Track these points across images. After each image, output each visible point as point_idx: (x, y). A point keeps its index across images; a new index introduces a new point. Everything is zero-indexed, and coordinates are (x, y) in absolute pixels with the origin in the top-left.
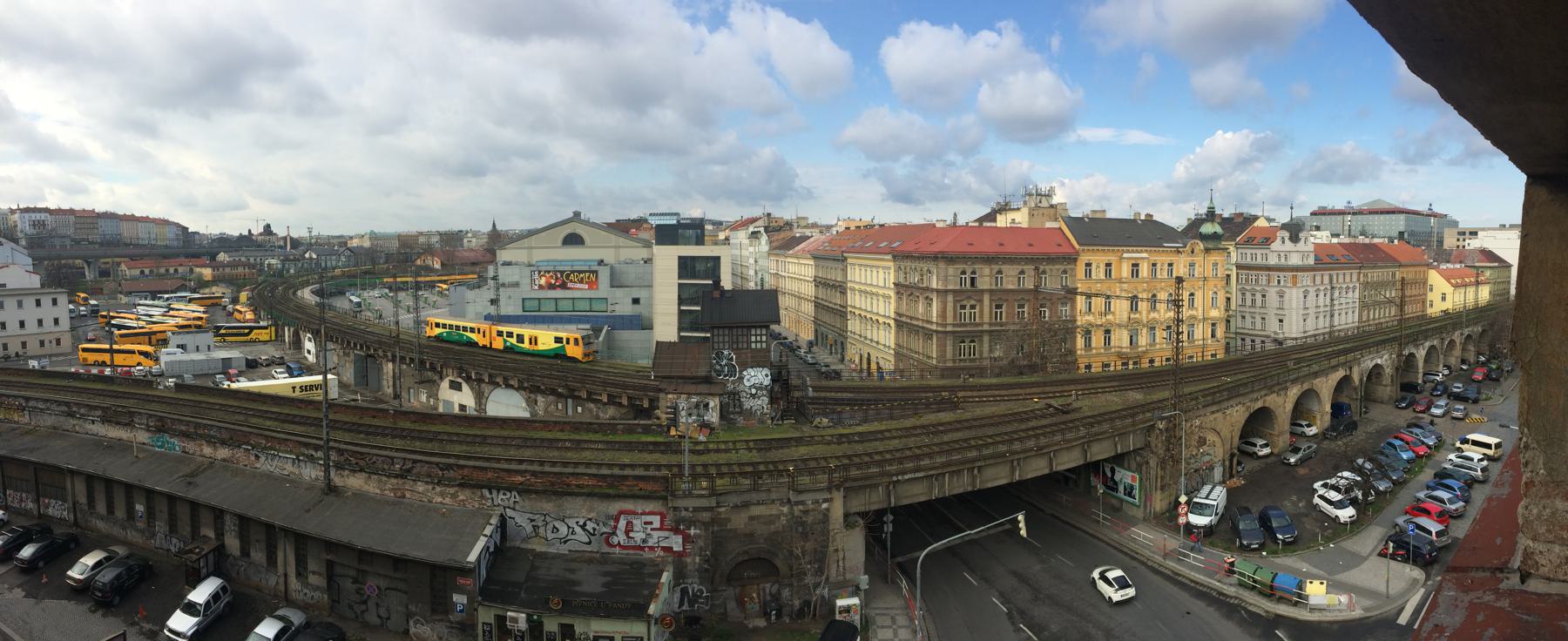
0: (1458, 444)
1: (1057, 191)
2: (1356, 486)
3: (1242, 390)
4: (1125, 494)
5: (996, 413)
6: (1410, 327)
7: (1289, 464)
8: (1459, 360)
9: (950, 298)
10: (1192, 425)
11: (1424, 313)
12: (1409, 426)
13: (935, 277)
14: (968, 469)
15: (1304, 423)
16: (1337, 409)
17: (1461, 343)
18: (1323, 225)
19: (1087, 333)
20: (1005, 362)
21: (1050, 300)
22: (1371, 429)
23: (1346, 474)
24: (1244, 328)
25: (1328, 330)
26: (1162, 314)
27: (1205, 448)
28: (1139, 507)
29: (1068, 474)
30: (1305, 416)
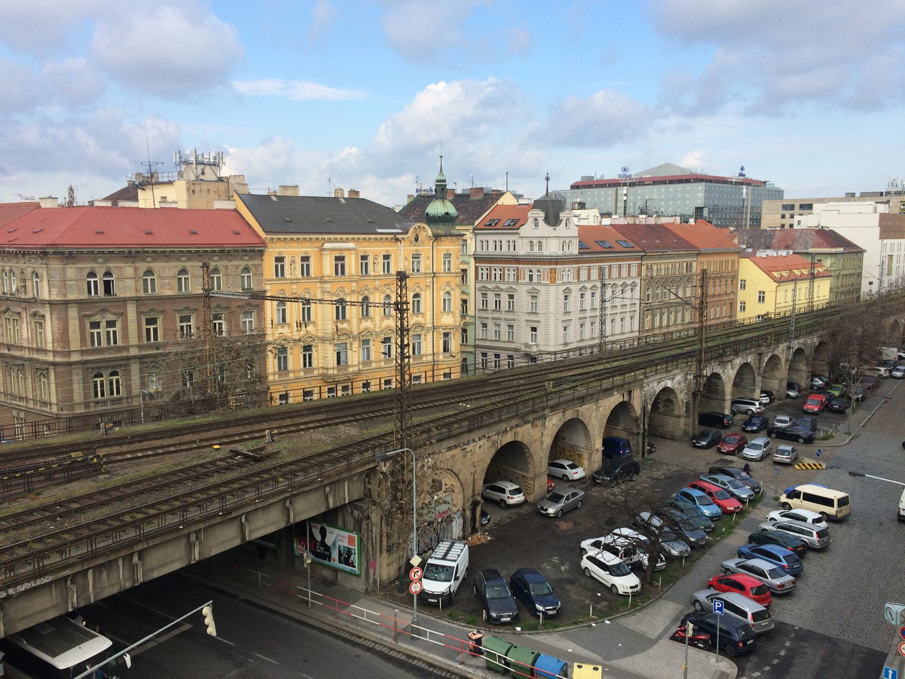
0: (783, 498)
2: (640, 547)
3: (487, 420)
4: (340, 562)
5: (158, 472)
6: (713, 338)
8: (785, 383)
9: (73, 313)
10: (423, 466)
11: (733, 319)
12: (712, 471)
13: (45, 283)
14: (124, 558)
15: (566, 463)
16: (611, 446)
17: (787, 360)
18: (588, 202)
19: (282, 351)
20: (166, 399)
22: (658, 474)
23: (626, 531)
24: (486, 340)
25: (597, 341)
26: (377, 322)
27: (441, 494)
29: (263, 543)
30: (568, 453)
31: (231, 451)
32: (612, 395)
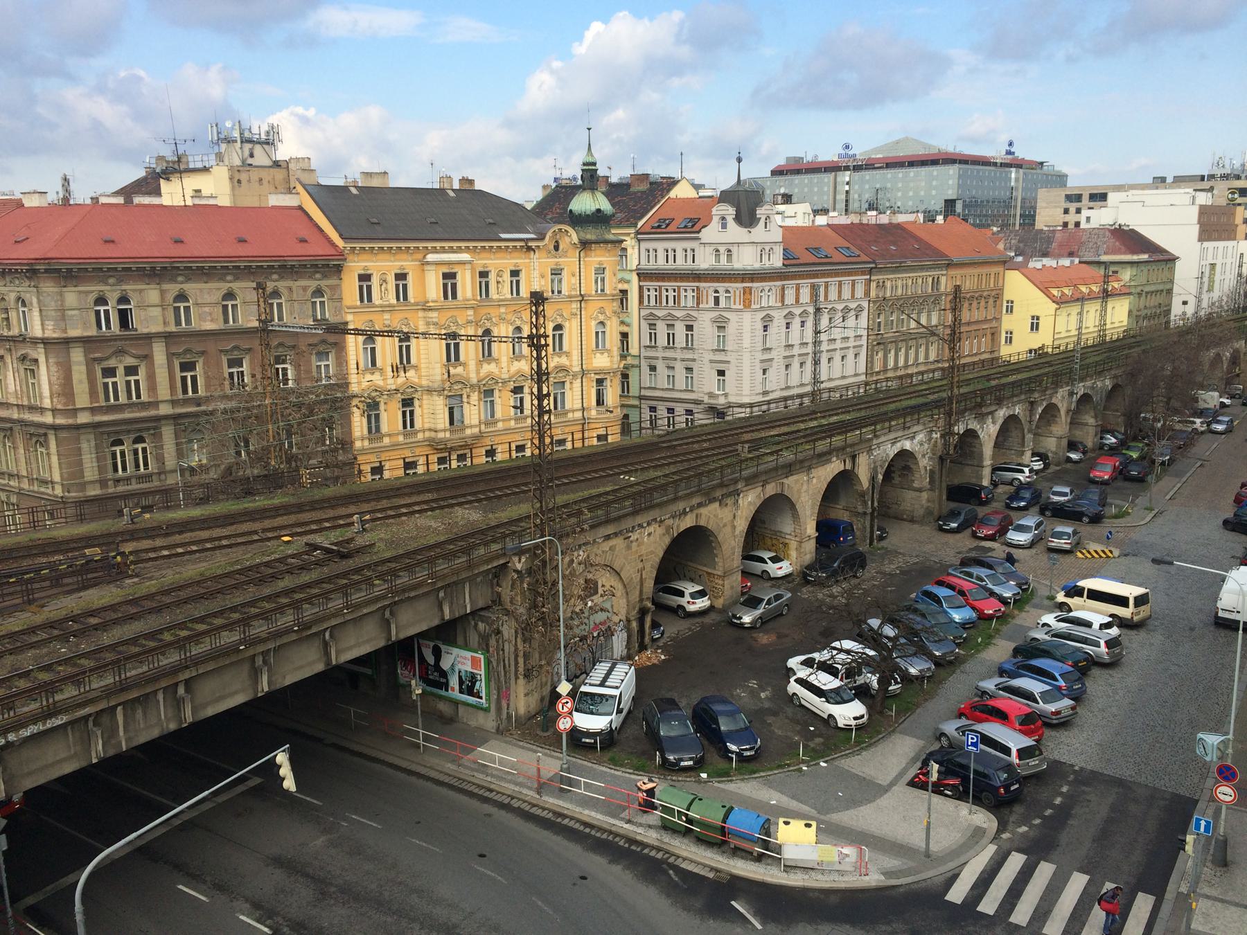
0: (1061, 597)
1: (285, 135)
4: (461, 692)
5: (208, 574)
6: (968, 382)
7: (741, 626)
8: (1065, 442)
9: (77, 355)
10: (572, 561)
11: (995, 355)
12: (965, 563)
13: (36, 313)
14: (165, 689)
15: (766, 555)
16: (828, 531)
17: (1068, 411)
18: (795, 191)
19: (372, 408)
20: (213, 475)
21: (294, 347)
22: (890, 567)
23: (848, 644)
24: (655, 388)
25: (809, 389)
26: (504, 364)
28: (487, 710)
30: (769, 542)
31: (307, 544)
32: (829, 461)
